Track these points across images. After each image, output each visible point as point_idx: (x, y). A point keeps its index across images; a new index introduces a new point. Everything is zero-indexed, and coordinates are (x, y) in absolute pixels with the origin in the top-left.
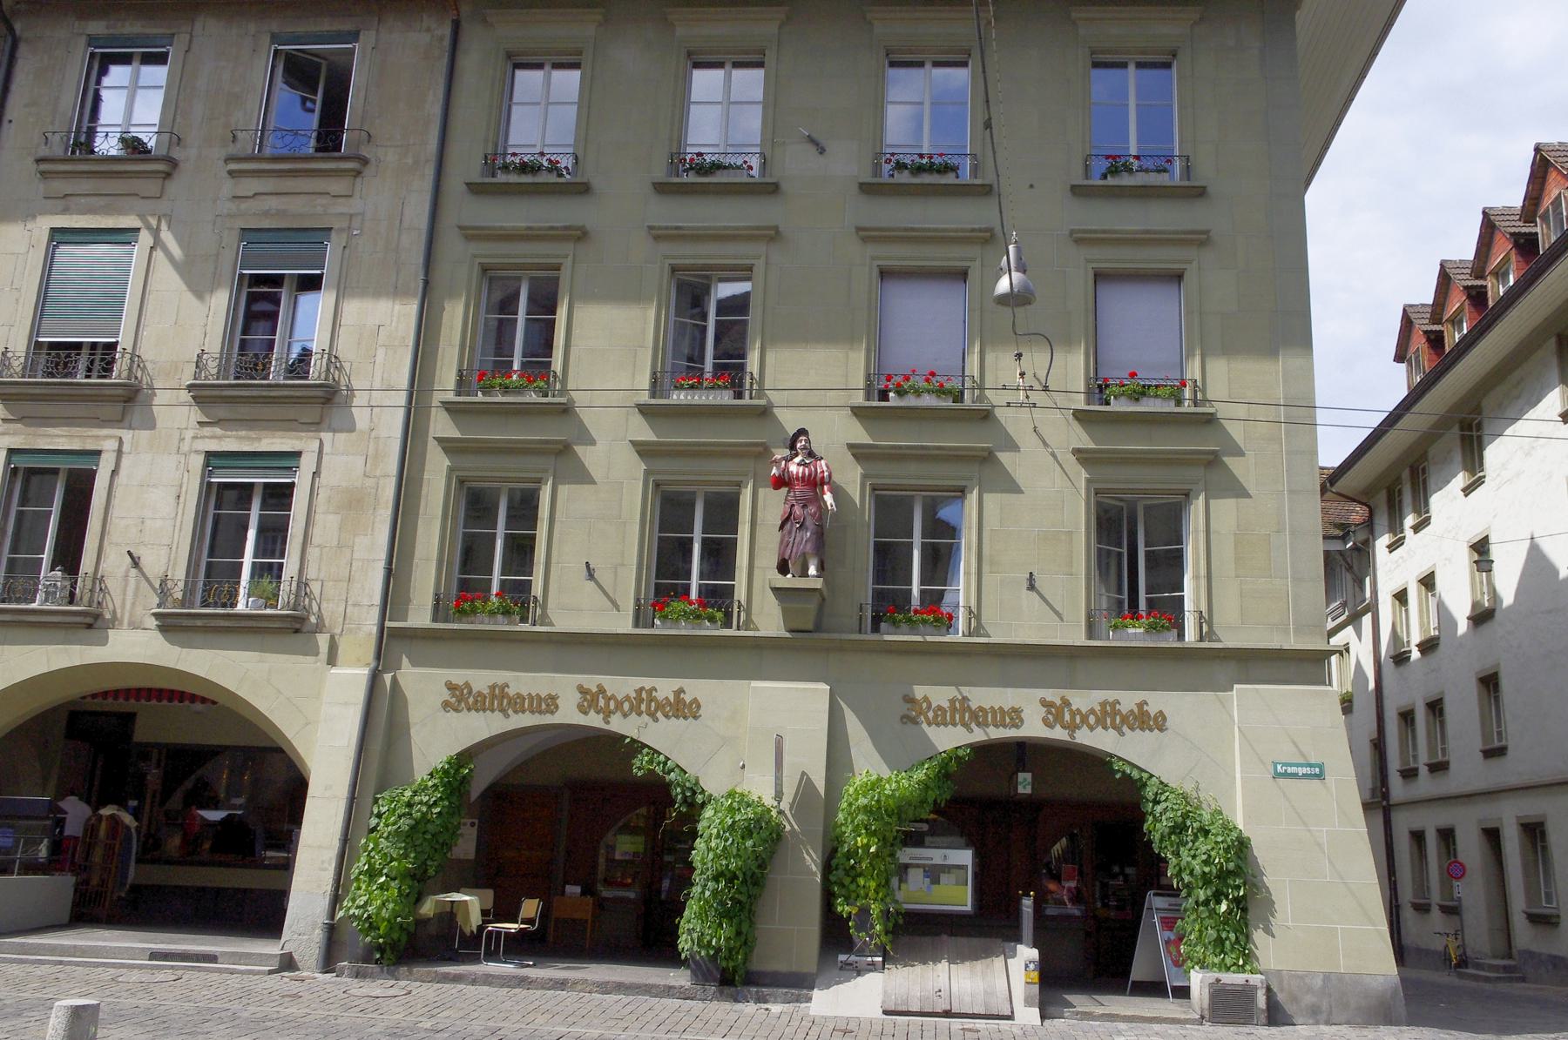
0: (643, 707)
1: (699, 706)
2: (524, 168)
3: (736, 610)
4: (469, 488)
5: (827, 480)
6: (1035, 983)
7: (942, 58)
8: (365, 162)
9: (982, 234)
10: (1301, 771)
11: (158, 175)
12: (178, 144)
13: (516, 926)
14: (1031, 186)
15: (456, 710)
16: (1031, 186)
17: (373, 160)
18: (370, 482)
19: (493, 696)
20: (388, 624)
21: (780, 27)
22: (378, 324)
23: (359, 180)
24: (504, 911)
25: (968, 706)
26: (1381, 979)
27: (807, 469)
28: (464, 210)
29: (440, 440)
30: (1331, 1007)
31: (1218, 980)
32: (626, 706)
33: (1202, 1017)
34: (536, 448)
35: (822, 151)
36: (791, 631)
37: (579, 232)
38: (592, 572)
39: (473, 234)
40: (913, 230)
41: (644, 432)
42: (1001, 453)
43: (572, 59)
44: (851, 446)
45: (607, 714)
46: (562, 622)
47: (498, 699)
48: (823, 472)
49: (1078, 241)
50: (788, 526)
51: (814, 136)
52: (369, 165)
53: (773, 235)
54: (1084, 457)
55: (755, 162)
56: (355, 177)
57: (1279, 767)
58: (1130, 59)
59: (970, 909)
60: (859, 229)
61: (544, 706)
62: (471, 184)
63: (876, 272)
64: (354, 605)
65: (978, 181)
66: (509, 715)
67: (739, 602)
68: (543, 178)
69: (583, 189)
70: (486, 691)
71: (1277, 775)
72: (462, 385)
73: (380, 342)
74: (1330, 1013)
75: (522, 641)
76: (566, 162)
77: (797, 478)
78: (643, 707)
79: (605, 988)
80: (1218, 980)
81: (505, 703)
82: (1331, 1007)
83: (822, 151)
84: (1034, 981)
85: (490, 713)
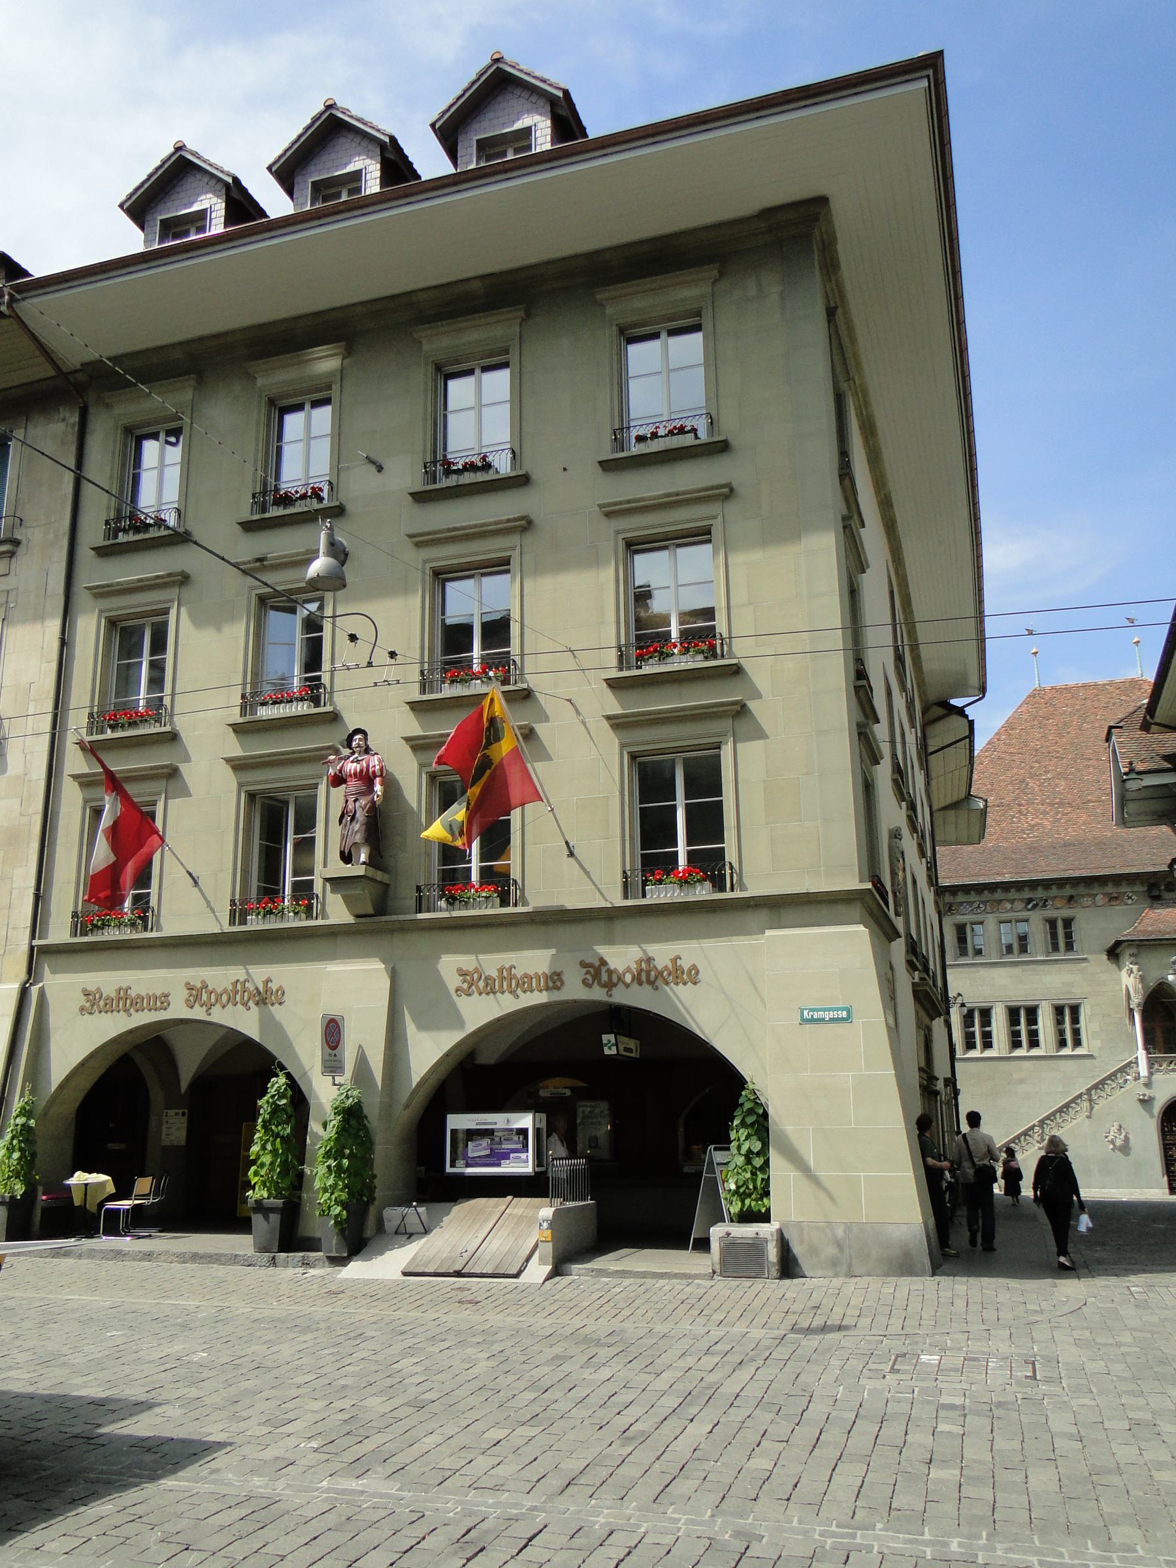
0: (238, 998)
1: (697, 973)
2: (470, 467)
3: (728, 871)
4: (639, 763)
5: (378, 773)
6: (549, 1241)
7: (684, 323)
8: (16, 543)
9: (517, 523)
10: (828, 1016)
11: (6, 555)
12: (21, 525)
13: (130, 1202)
14: (565, 469)
15: (91, 1013)
16: (565, 469)
17: (24, 541)
18: (25, 820)
19: (502, 978)
20: (36, 942)
21: (343, 360)
22: (29, 681)
23: (14, 559)
24: (123, 1191)
25: (654, 966)
26: (904, 1228)
27: (358, 765)
28: (93, 572)
29: (75, 777)
30: (851, 1259)
31: (728, 1234)
32: (225, 998)
33: (714, 1272)
34: (150, 775)
35: (380, 469)
36: (357, 916)
37: (523, 522)
38: (572, 849)
39: (102, 592)
40: (455, 529)
41: (235, 749)
42: (538, 725)
43: (502, 359)
44: (408, 739)
45: (209, 1007)
46: (755, 888)
47: (124, 1001)
48: (375, 766)
49: (608, 515)
50: (344, 821)
51: (373, 456)
52: (21, 546)
53: (727, 493)
54: (617, 723)
55: (702, 425)
56: (11, 557)
57: (805, 1013)
58: (660, 328)
59: (531, 1171)
60: (410, 536)
61: (158, 1004)
62: (243, 523)
63: (621, 545)
64: (14, 928)
65: (715, 439)
66: (518, 996)
67: (730, 863)
68: (153, 533)
69: (721, 448)
70: (113, 995)
71: (804, 1021)
72: (95, 724)
73: (31, 698)
74: (850, 1266)
75: (138, 947)
76: (171, 519)
77: (350, 775)
78: (238, 998)
79: (183, 1258)
80: (728, 1234)
81: (513, 986)
82: (851, 1259)
83: (380, 469)
84: (547, 1239)
85: (501, 995)
